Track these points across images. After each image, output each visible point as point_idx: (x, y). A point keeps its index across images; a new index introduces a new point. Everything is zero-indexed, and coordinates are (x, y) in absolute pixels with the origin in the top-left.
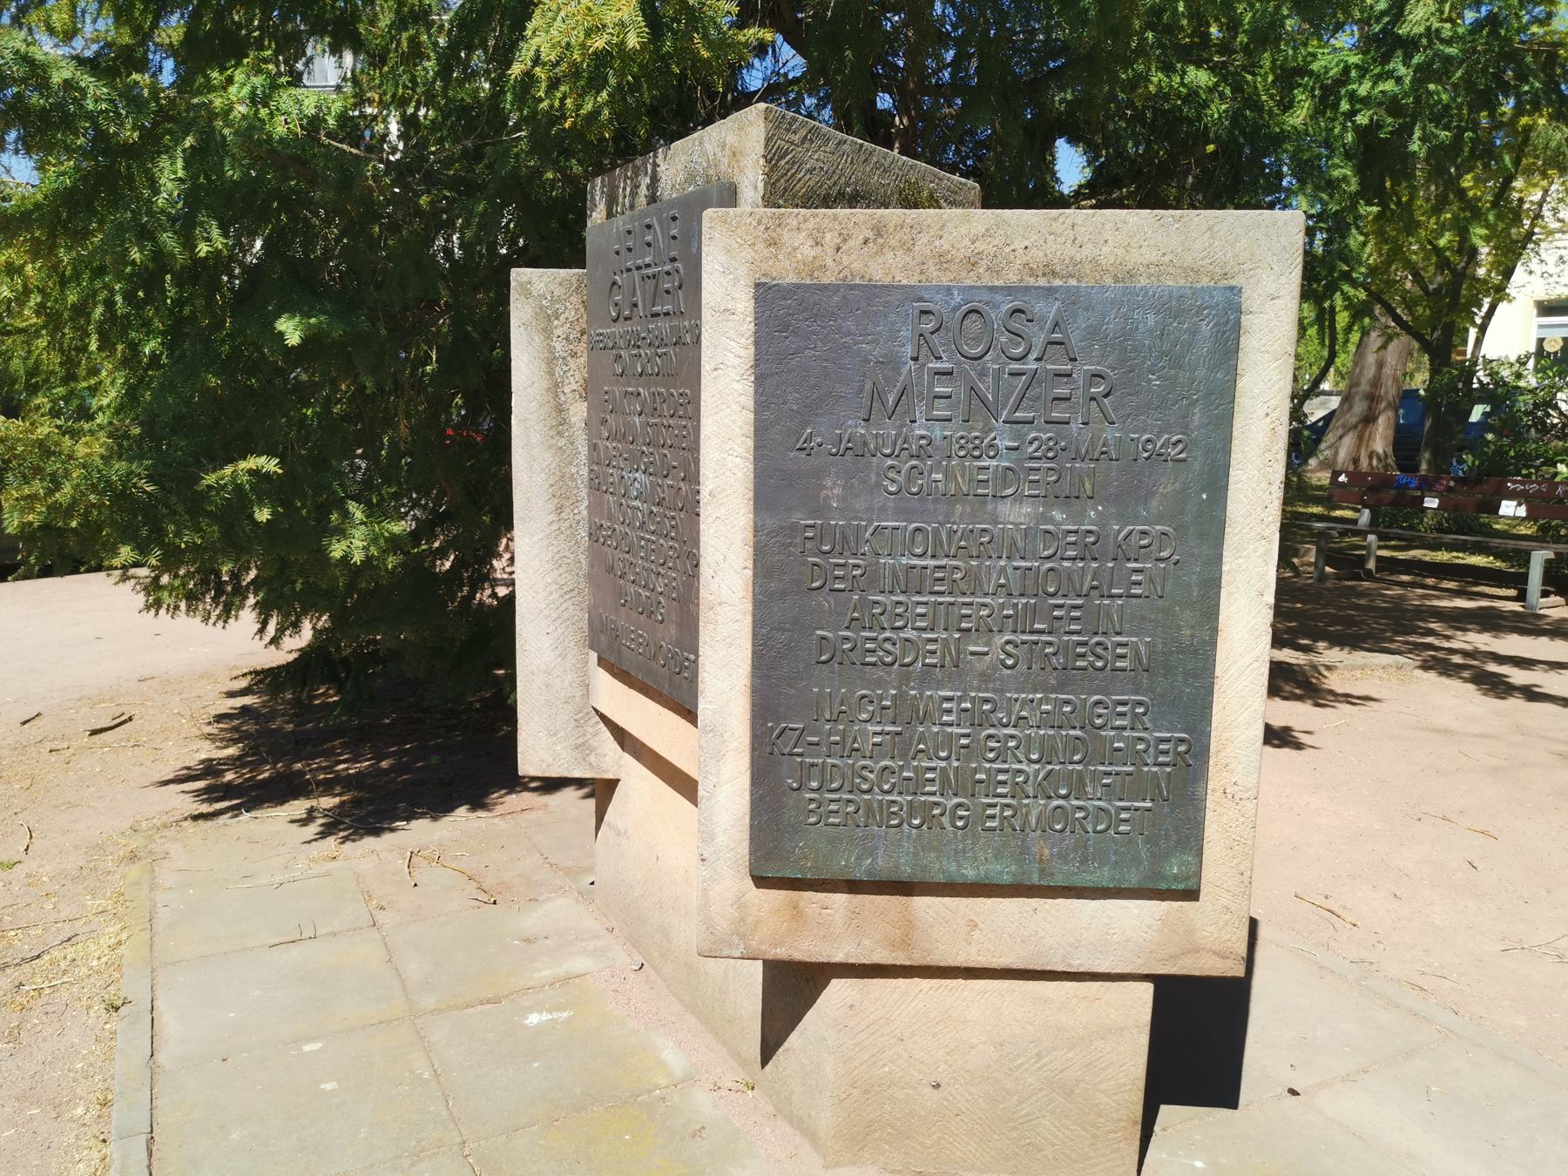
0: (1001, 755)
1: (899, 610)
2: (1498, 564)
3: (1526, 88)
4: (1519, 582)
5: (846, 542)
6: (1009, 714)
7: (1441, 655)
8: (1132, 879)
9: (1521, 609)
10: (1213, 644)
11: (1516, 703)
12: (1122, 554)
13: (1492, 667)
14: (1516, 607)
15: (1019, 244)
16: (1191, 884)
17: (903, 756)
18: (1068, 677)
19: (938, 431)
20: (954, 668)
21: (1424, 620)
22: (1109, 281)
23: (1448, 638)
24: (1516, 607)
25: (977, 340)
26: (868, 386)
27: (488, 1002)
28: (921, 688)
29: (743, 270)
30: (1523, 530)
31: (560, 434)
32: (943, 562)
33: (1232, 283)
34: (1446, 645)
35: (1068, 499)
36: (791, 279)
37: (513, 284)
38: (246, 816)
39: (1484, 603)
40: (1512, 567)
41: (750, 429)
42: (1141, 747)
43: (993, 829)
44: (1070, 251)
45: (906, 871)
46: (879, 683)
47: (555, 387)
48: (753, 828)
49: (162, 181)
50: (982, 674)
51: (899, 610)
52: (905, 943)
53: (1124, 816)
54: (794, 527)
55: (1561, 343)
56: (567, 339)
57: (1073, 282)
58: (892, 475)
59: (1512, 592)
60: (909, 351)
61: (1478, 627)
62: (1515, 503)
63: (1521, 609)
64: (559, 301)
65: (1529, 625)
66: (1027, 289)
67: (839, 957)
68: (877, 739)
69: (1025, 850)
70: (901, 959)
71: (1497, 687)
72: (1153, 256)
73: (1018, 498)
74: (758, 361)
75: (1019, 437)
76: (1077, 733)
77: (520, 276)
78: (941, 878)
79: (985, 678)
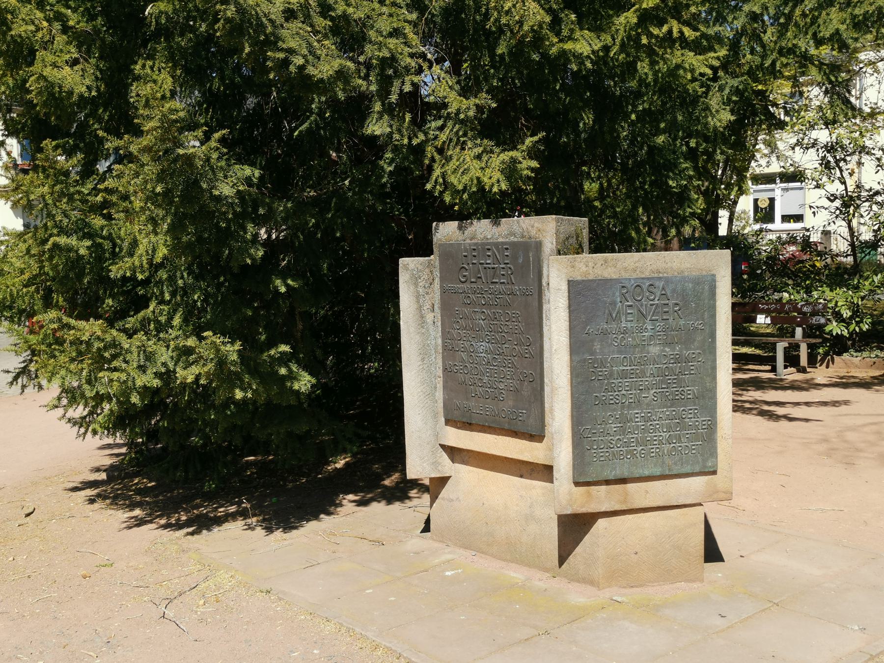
0: (655, 431)
1: (620, 385)
2: (758, 352)
3: (758, 119)
5: (602, 364)
6: (656, 416)
9: (774, 377)
10: (716, 387)
11: (784, 423)
12: (687, 361)
13: (766, 408)
14: (771, 375)
15: (649, 264)
16: (715, 469)
17: (624, 434)
18: (674, 402)
19: (629, 325)
22: (676, 274)
23: (740, 395)
24: (771, 375)
25: (639, 295)
26: (607, 311)
27: (423, 571)
28: (628, 410)
29: (563, 276)
32: (633, 367)
33: (712, 273)
34: (740, 398)
35: (670, 344)
36: (579, 278)
38: (195, 536)
40: (766, 352)
42: (697, 424)
43: (653, 457)
44: (664, 265)
45: (626, 474)
46: (615, 410)
47: (420, 308)
48: (574, 465)
49: (248, 228)
50: (647, 404)
51: (620, 385)
52: (625, 501)
53: (693, 447)
54: (585, 360)
55: (768, 202)
56: (424, 287)
57: (665, 275)
58: (616, 340)
59: (768, 368)
60: (619, 299)
61: (754, 389)
62: (764, 316)
63: (774, 377)
64: (420, 271)
66: (653, 278)
67: (603, 509)
68: (615, 429)
69: (663, 463)
70: (624, 507)
72: (689, 266)
73: (655, 345)
75: (653, 325)
76: (677, 421)
77: (403, 261)
78: (638, 476)
79: (648, 405)
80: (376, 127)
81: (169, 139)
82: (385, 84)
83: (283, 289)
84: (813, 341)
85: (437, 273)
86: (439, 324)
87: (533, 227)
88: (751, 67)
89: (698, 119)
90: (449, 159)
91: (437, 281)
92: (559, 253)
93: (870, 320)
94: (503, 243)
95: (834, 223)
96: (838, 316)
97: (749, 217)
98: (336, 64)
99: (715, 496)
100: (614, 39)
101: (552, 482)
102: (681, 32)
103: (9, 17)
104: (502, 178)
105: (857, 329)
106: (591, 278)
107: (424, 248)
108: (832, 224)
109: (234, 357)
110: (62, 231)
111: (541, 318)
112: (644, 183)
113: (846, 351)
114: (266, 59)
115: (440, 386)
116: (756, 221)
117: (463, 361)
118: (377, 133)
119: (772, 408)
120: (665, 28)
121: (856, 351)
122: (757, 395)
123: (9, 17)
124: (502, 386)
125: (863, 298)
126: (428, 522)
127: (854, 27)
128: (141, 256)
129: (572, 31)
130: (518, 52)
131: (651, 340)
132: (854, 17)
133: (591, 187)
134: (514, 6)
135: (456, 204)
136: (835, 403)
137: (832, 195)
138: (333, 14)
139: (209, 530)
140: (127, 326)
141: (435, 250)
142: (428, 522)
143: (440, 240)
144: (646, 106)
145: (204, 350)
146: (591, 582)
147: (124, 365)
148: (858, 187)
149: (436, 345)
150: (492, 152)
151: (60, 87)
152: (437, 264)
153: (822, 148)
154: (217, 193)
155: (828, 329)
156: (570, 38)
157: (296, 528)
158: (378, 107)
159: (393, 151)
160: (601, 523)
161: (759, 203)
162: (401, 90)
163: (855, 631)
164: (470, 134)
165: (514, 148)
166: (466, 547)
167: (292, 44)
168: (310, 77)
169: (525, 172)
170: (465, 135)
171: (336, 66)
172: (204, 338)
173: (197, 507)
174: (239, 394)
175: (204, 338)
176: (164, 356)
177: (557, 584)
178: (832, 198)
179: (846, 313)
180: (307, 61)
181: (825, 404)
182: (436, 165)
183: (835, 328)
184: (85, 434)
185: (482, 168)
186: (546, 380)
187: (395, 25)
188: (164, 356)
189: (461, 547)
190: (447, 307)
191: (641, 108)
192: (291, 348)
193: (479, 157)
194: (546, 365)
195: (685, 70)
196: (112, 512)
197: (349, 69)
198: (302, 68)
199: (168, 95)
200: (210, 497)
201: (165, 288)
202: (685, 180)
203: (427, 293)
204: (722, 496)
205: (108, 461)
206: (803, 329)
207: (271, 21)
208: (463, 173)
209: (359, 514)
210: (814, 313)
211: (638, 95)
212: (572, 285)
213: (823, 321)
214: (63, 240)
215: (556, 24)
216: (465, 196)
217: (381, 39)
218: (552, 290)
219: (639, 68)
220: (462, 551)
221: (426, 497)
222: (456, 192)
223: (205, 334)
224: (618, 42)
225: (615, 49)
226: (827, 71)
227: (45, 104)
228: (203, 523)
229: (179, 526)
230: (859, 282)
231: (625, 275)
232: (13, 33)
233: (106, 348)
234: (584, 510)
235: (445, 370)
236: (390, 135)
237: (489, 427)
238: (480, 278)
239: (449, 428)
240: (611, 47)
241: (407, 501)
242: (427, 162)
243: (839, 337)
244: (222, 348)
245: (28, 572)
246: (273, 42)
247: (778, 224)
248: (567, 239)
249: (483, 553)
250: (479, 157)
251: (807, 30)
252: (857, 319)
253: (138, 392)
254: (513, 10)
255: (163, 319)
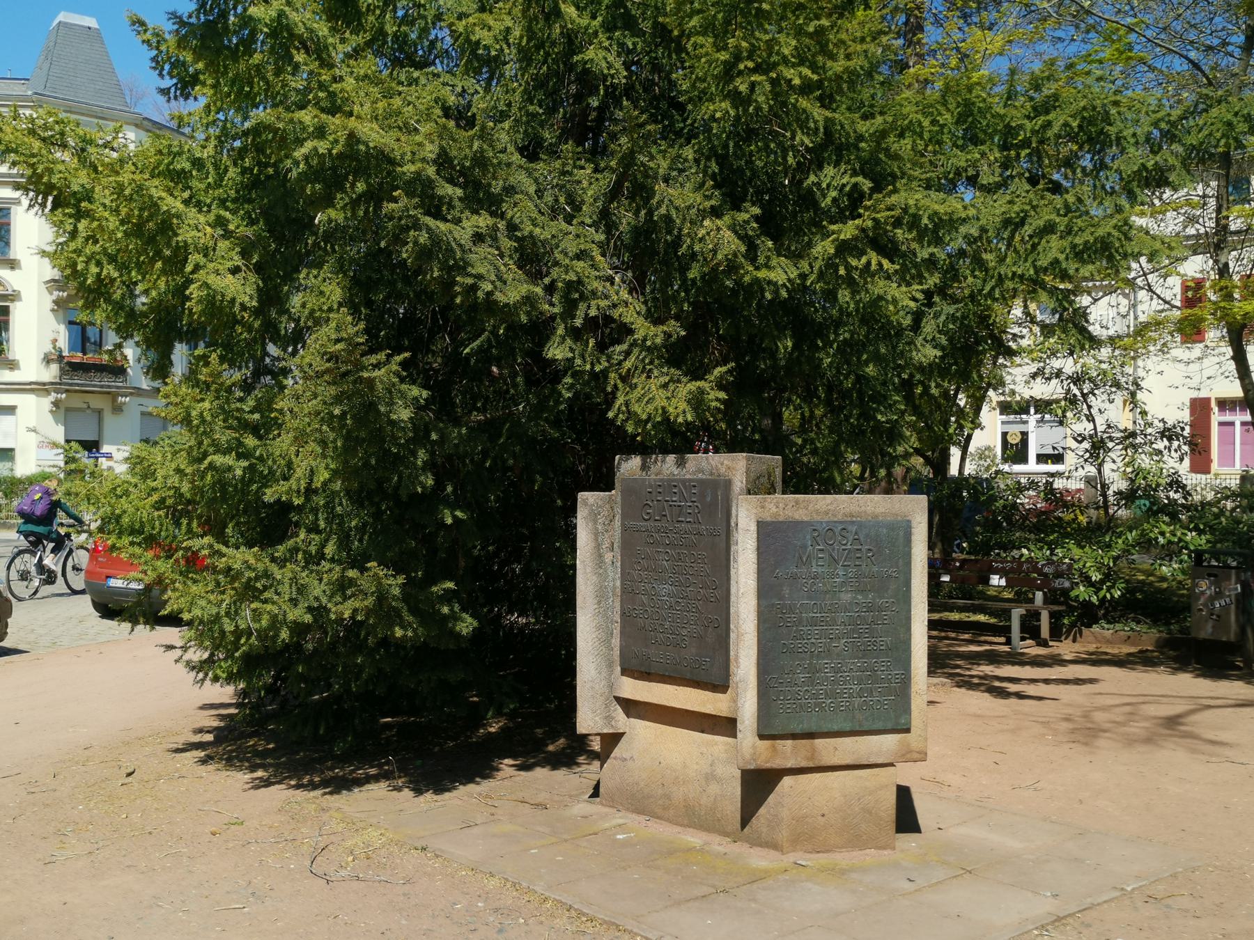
2: (993, 621)
4: (1005, 631)
5: (791, 609)
7: (966, 679)
8: (889, 726)
13: (997, 684)
14: (1006, 648)
17: (812, 685)
19: (820, 570)
20: (828, 653)
21: (950, 659)
23: (969, 669)
24: (1006, 648)
25: (831, 539)
30: (1006, 595)
31: (600, 567)
34: (968, 673)
36: (769, 519)
37: (579, 500)
39: (987, 647)
41: (756, 571)
45: (814, 729)
46: (803, 659)
47: (598, 546)
52: (812, 758)
54: (773, 604)
59: (1002, 640)
60: (809, 543)
64: (600, 507)
65: (1016, 659)
66: (845, 522)
67: (789, 766)
69: (854, 717)
71: (1002, 694)
73: (847, 592)
74: (758, 549)
77: (583, 496)
78: (826, 730)
79: (838, 655)
80: (557, 351)
81: (351, 362)
82: (570, 308)
83: (449, 521)
84: (1056, 608)
85: (618, 510)
86: (619, 564)
87: (722, 464)
88: (973, 291)
89: (902, 352)
90: (633, 387)
91: (618, 517)
92: (749, 493)
93: (1123, 585)
94: (690, 480)
95: (1082, 467)
96: (1087, 580)
97: (995, 455)
98: (524, 289)
99: (908, 756)
100: (811, 267)
101: (735, 737)
102: (880, 265)
103: (175, 221)
104: (688, 409)
105: (1108, 596)
106: (781, 519)
107: (604, 481)
108: (1080, 469)
109: (396, 591)
110: (219, 450)
111: (728, 560)
112: (851, 415)
113: (1097, 622)
114: (454, 283)
115: (617, 632)
116: (1005, 460)
117: (643, 604)
118: (559, 357)
119: (1004, 685)
120: (864, 260)
121: (1109, 622)
122: (988, 669)
123: (175, 221)
124: (684, 632)
125: (1116, 559)
126: (597, 788)
127: (1076, 257)
128: (299, 480)
129: (768, 258)
130: (712, 277)
131: (842, 587)
132: (1074, 246)
133: (791, 417)
134: (708, 234)
135: (638, 434)
136: (1078, 682)
137: (1080, 435)
138: (519, 234)
139: (349, 790)
140: (276, 555)
141: (617, 485)
142: (597, 788)
143: (623, 474)
144: (847, 335)
145: (365, 582)
146: (774, 846)
147: (276, 598)
148: (1109, 426)
149: (614, 587)
150: (679, 381)
151: (223, 295)
152: (619, 499)
153: (1067, 379)
154: (394, 417)
155: (1073, 594)
156: (767, 266)
157: (449, 790)
158: (560, 331)
159: (573, 376)
160: (787, 781)
161: (1008, 437)
162: (587, 315)
163: (1046, 897)
164: (656, 362)
165: (701, 378)
166: (640, 811)
167: (481, 269)
168: (496, 302)
169: (714, 404)
170: (651, 363)
171: (524, 291)
172: (368, 569)
173: (332, 769)
174: (399, 632)
175: (368, 569)
176: (318, 590)
177: (740, 849)
178: (1080, 438)
179: (1096, 576)
180: (495, 287)
181: (1066, 682)
182: (619, 394)
183: (1082, 592)
184: (203, 680)
185: (668, 398)
186: (732, 626)
187: (582, 247)
188: (318, 590)
189: (633, 812)
190: (628, 546)
191: (841, 338)
192: (456, 585)
193: (665, 386)
194: (732, 610)
195: (887, 302)
196: (228, 773)
197: (537, 295)
198: (489, 294)
199: (335, 307)
200: (344, 759)
201: (320, 515)
202: (896, 414)
203: (607, 531)
204: (916, 756)
205: (216, 724)
206: (1045, 594)
207: (460, 245)
208: (647, 402)
209: (518, 778)
210: (1059, 575)
211: (838, 324)
212: (761, 525)
213: (1067, 584)
214: (219, 460)
215: (752, 249)
216: (649, 426)
217: (567, 261)
218: (740, 531)
219: (839, 296)
220: (634, 816)
221: (597, 763)
222: (639, 422)
223: (369, 565)
224: (816, 270)
225: (813, 277)
226: (1060, 297)
227: (202, 313)
228: (340, 785)
229: (313, 786)
230: (1111, 540)
231: (817, 518)
232: (180, 238)
233: (257, 578)
234: (768, 765)
235: (623, 614)
236: (570, 361)
237: (670, 677)
238: (665, 516)
239: (625, 679)
240: (807, 275)
241: (574, 767)
242: (609, 389)
243: (1087, 605)
244: (384, 581)
245: (149, 829)
246: (462, 268)
247: (1032, 466)
248: (758, 478)
249: (658, 818)
250: (665, 386)
251: (1027, 256)
252: (1108, 584)
253: (288, 627)
254: (707, 237)
255: (313, 549)
